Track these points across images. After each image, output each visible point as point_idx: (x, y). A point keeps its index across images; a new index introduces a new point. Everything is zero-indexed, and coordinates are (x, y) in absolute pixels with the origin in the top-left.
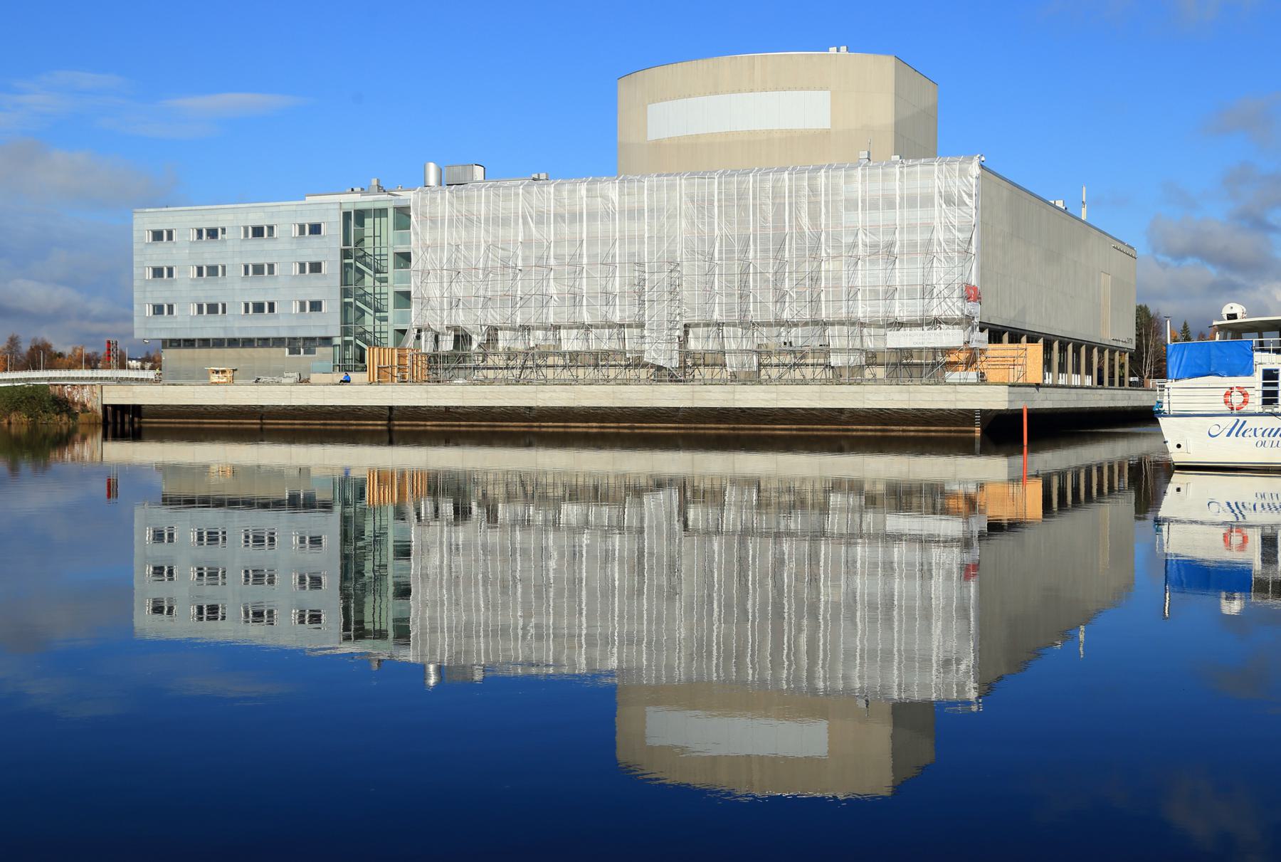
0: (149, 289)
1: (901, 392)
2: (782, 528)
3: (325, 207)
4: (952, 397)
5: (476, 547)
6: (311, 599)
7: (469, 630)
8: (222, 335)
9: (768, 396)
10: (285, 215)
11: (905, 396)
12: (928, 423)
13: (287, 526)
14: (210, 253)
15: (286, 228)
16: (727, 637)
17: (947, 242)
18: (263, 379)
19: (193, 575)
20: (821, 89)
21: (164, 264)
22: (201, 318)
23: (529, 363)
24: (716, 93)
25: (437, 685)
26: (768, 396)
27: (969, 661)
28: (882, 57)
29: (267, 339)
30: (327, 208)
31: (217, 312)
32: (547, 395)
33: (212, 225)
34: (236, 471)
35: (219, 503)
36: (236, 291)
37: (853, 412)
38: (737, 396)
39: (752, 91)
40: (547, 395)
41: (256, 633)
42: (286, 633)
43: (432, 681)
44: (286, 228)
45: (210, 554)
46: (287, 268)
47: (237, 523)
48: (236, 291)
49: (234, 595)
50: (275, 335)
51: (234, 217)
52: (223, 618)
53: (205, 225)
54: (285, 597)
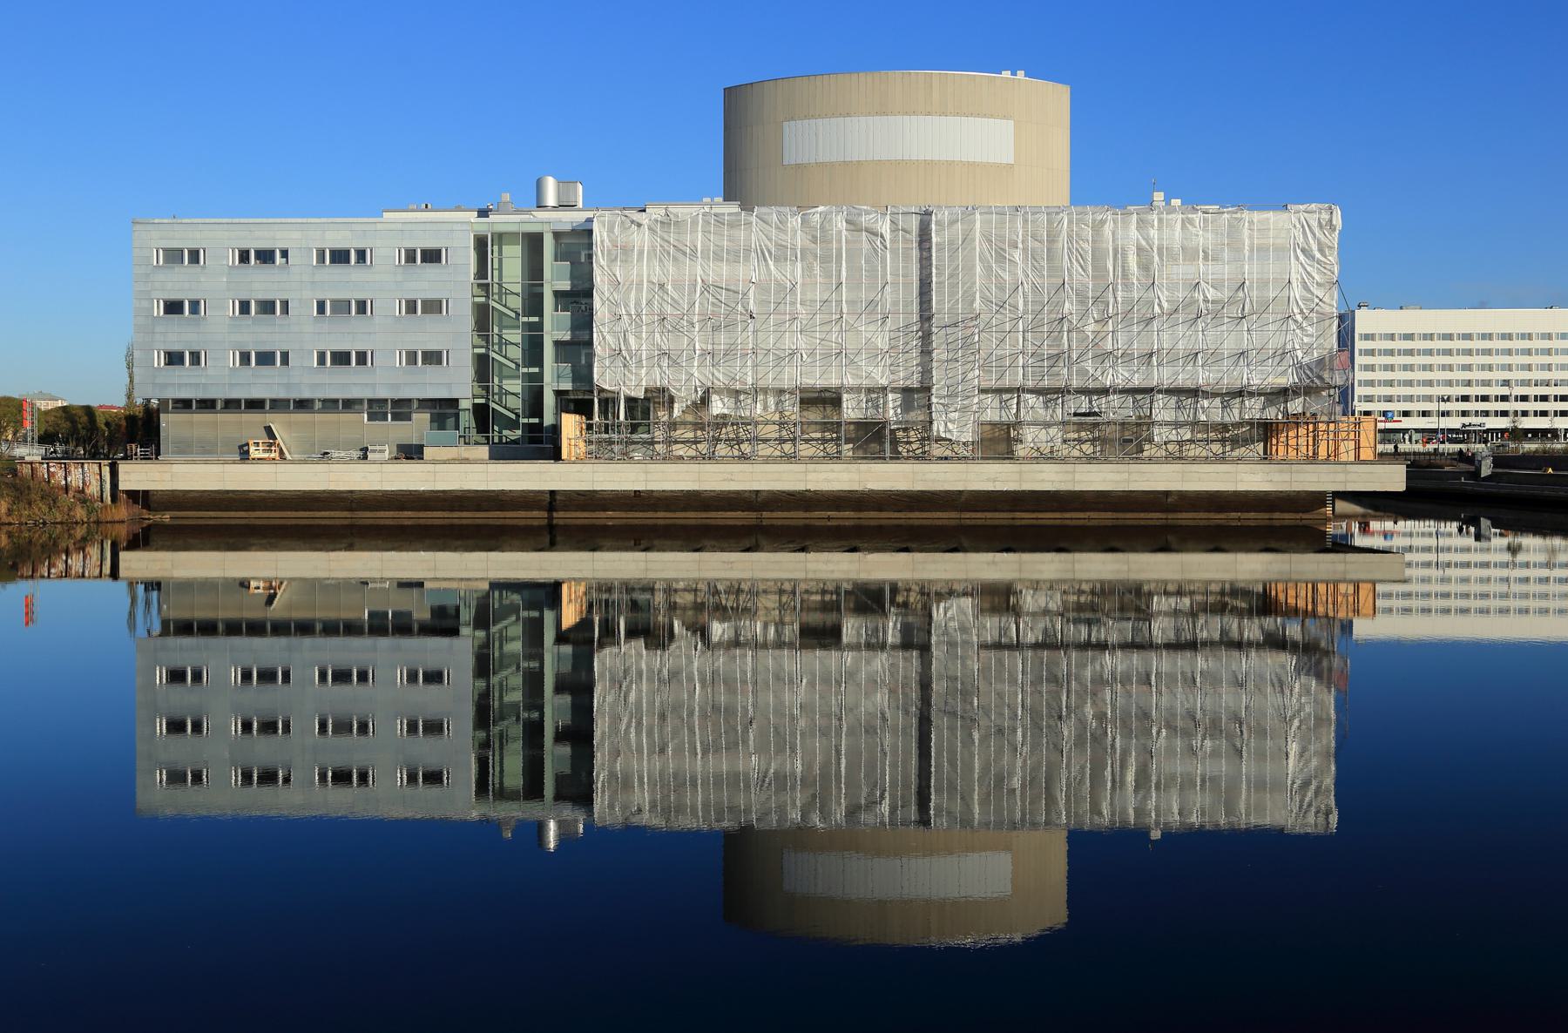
0: (158, 329)
1: (1281, 471)
2: (1093, 639)
3: (409, 227)
4: (1341, 477)
5: (690, 679)
6: (427, 751)
7: (680, 782)
8: (282, 395)
9: (1117, 477)
10: (392, 230)
11: (1287, 477)
12: (1220, 509)
13: (389, 657)
14: (261, 283)
15: (386, 253)
16: (1035, 769)
17: (1304, 299)
18: (335, 454)
19: (235, 727)
20: (1005, 117)
21: (186, 296)
22: (246, 370)
23: (716, 433)
24: (885, 114)
25: (559, 847)
26: (1117, 477)
27: (1329, 781)
28: (1060, 86)
29: (336, 401)
30: (455, 229)
31: (273, 363)
32: (823, 476)
33: (265, 245)
34: (312, 586)
35: (281, 628)
36: (304, 336)
37: (1183, 495)
38: (1077, 477)
39: (929, 114)
40: (823, 476)
41: (424, 803)
42: (390, 798)
43: (552, 842)
44: (386, 253)
45: (265, 700)
46: (388, 306)
47: (308, 656)
48: (304, 336)
49: (305, 751)
50: (201, 395)
51: (302, 236)
52: (287, 780)
53: (253, 245)
54: (387, 753)
